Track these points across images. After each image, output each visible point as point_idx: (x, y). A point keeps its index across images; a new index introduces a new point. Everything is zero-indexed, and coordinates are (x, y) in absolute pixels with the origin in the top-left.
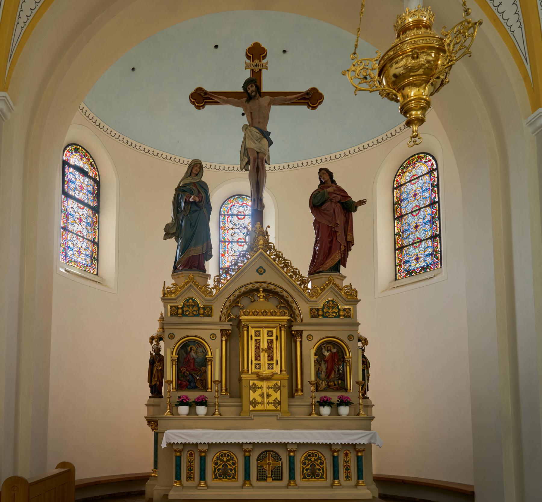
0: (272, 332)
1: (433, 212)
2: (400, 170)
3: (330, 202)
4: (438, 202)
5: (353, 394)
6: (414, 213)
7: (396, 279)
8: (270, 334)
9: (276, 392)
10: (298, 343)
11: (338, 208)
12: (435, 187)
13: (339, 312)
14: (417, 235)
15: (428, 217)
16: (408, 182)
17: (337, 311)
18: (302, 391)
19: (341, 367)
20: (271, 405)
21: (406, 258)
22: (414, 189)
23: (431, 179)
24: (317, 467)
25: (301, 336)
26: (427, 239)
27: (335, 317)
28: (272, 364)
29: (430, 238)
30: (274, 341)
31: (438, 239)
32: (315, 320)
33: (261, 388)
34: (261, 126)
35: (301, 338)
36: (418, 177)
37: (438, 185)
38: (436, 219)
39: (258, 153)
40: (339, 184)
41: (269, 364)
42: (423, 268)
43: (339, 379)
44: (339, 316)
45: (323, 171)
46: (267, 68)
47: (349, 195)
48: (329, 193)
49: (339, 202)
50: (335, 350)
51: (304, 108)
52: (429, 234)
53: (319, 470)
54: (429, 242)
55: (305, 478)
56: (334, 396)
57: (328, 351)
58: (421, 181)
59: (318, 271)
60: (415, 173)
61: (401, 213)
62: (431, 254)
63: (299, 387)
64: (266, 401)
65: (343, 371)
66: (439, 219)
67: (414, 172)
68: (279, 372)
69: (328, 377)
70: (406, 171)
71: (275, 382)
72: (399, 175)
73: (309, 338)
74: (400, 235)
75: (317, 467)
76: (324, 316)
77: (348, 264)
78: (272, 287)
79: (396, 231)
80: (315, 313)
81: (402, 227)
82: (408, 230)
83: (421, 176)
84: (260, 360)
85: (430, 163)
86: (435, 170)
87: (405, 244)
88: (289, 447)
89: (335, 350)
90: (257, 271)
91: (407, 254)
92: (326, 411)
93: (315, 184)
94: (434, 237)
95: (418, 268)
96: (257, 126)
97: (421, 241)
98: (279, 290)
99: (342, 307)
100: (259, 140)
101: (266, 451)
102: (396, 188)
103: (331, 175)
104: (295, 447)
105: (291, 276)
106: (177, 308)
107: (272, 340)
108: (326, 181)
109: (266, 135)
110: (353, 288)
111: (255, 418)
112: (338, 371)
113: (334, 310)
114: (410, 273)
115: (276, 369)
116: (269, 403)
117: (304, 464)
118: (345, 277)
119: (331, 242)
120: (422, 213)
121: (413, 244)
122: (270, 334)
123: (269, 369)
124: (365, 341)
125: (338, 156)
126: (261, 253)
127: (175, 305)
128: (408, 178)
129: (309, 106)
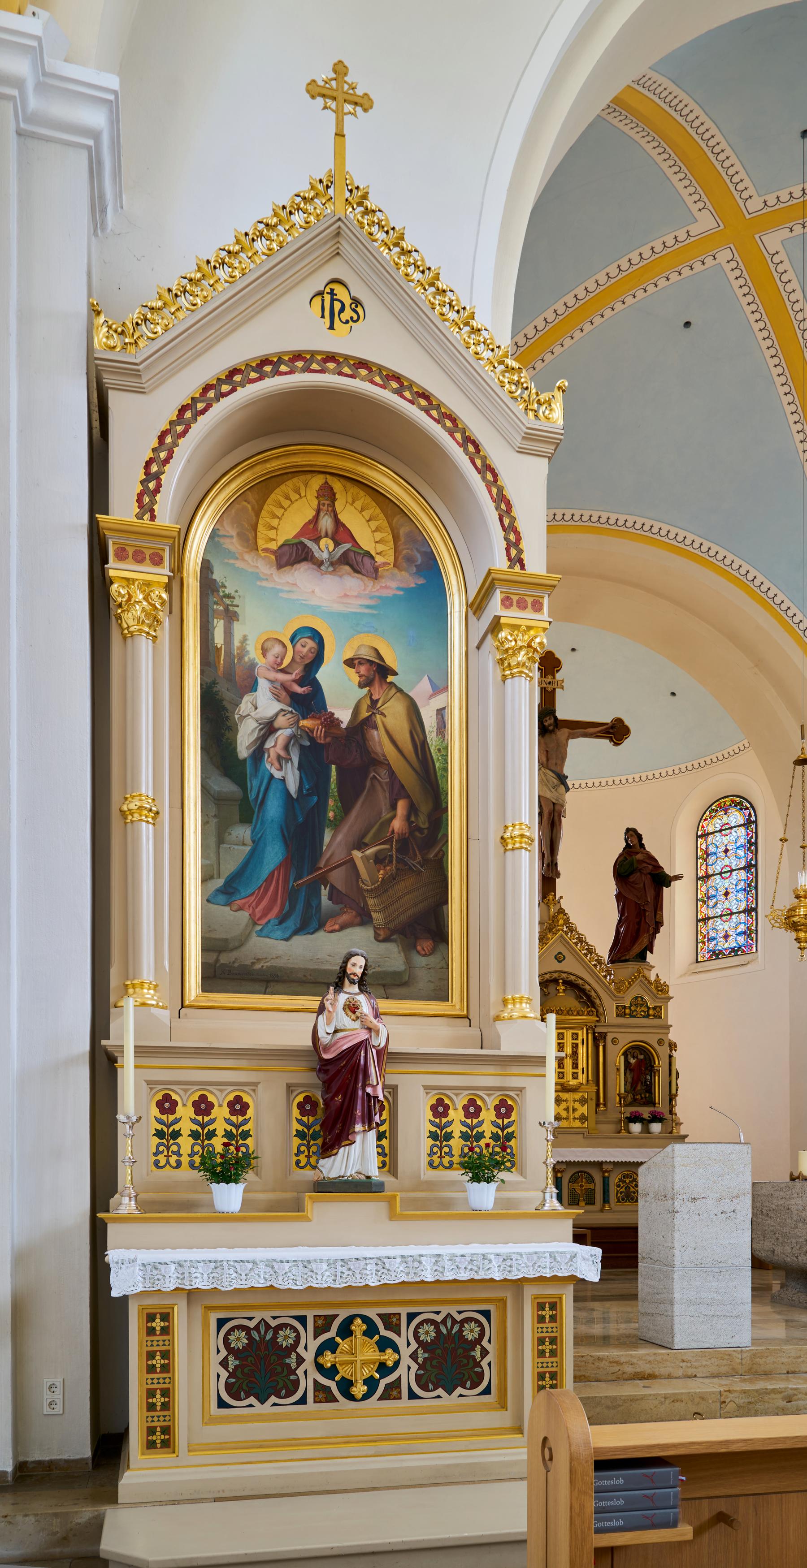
0: (577, 1034)
1: (748, 878)
2: (708, 813)
3: (638, 874)
4: (756, 866)
5: (661, 1107)
6: (723, 875)
7: (697, 962)
8: (575, 1036)
9: (583, 1106)
10: (601, 1048)
11: (648, 880)
12: (752, 845)
13: (648, 1011)
14: (727, 905)
15: (742, 884)
16: (717, 832)
17: (646, 1009)
18: (605, 1105)
19: (648, 1077)
20: (577, 1121)
21: (712, 934)
22: (726, 842)
23: (748, 834)
24: (632, 1189)
25: (605, 1039)
26: (740, 912)
27: (644, 1017)
28: (577, 1073)
29: (744, 911)
30: (580, 1045)
31: (754, 914)
32: (621, 1020)
33: (566, 1101)
34: (557, 769)
35: (605, 1041)
36: (731, 828)
37: (756, 844)
38: (752, 888)
39: (554, 804)
40: (648, 848)
41: (573, 1073)
42: (733, 950)
43: (646, 1092)
44: (648, 1016)
45: (631, 832)
46: (562, 688)
47: (661, 864)
48: (639, 861)
49: (650, 874)
50: (642, 1057)
51: (606, 742)
52: (743, 906)
53: (634, 1193)
54: (743, 916)
55: (619, 1201)
56: (645, 1112)
57: (634, 1057)
58: (734, 834)
59: (623, 958)
60: (727, 821)
61: (706, 872)
62: (745, 933)
63: (601, 1100)
64: (571, 1116)
65: (651, 1082)
66: (756, 888)
67: (725, 819)
68: (585, 1082)
69: (634, 1090)
70: (715, 816)
71: (581, 1094)
72: (706, 820)
73: (614, 1041)
74: (705, 902)
75: (632, 1189)
76: (632, 1016)
77: (655, 949)
78: (572, 978)
79: (700, 896)
80: (621, 1012)
81: (708, 891)
82: (715, 896)
83: (735, 827)
84: (563, 1068)
85: (747, 812)
86: (753, 822)
87: (711, 915)
88: (605, 1167)
89: (642, 1057)
90: (556, 958)
91: (713, 929)
92: (636, 1128)
93: (620, 845)
94: (748, 911)
95: (727, 949)
96: (553, 768)
97: (732, 914)
98: (580, 982)
99: (650, 1005)
100: (555, 787)
101: (578, 1172)
102: (702, 836)
103: (640, 837)
104: (610, 1167)
105: (595, 966)
106: (625, 1007)
107: (577, 1044)
108: (634, 845)
109: (562, 779)
110: (662, 982)
111: (560, 1136)
112: (645, 1082)
113: (643, 1009)
114: (716, 954)
115: (582, 1078)
116: (574, 1119)
117: (618, 1186)
118: (653, 967)
119: (639, 923)
120: (735, 877)
121: (721, 916)
122: (575, 1037)
123: (573, 1078)
124: (673, 1046)
125: (624, 781)
126: (561, 936)
127: (621, 1003)
128: (717, 826)
129: (611, 740)
